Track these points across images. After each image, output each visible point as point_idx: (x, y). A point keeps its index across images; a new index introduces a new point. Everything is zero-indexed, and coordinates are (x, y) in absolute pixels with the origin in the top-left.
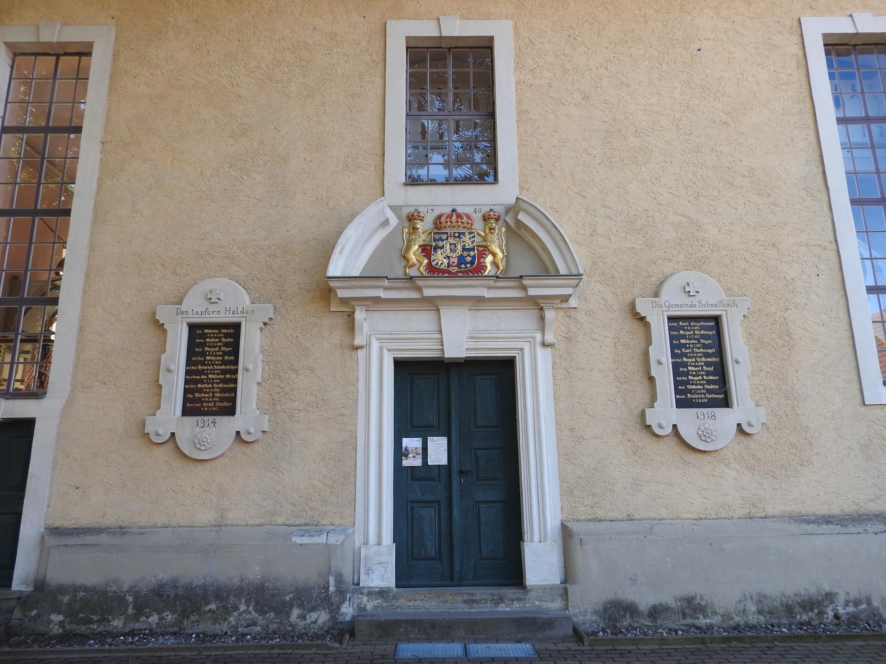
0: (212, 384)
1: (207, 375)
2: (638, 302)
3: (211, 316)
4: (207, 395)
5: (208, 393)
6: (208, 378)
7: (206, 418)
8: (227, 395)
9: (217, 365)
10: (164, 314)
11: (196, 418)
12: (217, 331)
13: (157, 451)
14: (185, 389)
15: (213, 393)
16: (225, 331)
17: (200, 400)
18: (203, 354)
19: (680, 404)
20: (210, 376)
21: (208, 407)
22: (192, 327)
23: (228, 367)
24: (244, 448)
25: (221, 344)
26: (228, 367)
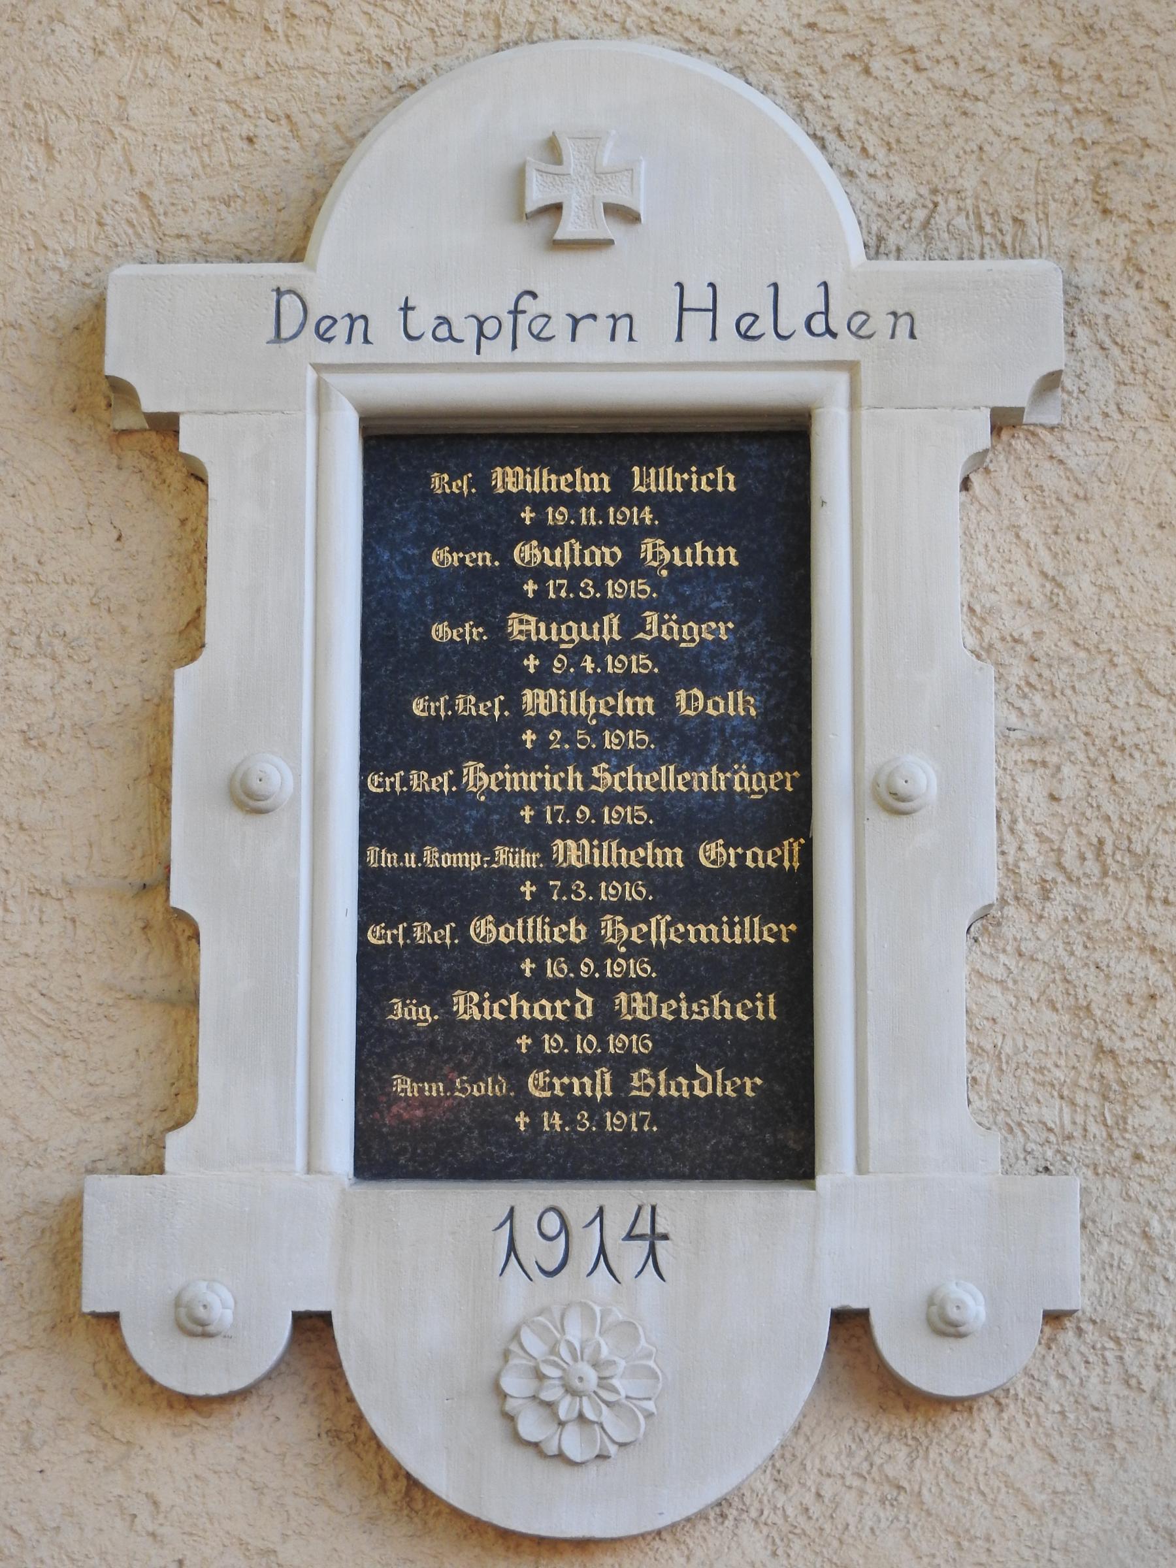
0: (591, 913)
1: (538, 838)
2: (126, 285)
3: (562, 349)
4: (549, 1010)
5: (560, 990)
6: (547, 871)
7: (579, 1199)
8: (718, 1008)
9: (622, 759)
10: (174, 335)
11: (494, 1198)
12: (596, 482)
13: (170, 1457)
14: (366, 955)
15: (604, 990)
16: (662, 480)
17: (495, 1049)
18: (498, 667)
19: (389, 1150)
20: (570, 853)
21: (568, 1105)
22: (399, 450)
23: (710, 780)
24: (890, 1449)
25: (640, 588)
26: (710, 780)
